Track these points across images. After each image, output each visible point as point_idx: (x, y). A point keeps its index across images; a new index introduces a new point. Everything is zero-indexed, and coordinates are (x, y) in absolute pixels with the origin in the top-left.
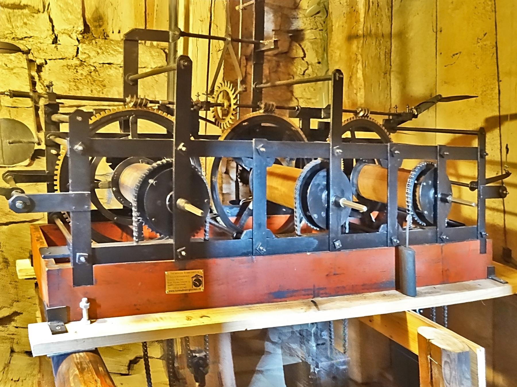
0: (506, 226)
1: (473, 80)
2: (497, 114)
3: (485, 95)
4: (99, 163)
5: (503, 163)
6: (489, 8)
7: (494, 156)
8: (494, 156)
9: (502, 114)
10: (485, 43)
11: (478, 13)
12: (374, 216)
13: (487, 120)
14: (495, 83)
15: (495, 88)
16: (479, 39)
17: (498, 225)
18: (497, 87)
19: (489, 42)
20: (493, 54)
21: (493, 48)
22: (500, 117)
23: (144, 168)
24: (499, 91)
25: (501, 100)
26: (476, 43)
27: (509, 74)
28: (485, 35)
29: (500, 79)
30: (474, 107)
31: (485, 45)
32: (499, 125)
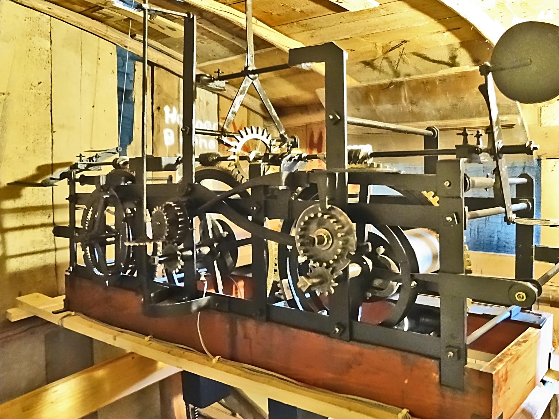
0: (57, 261)
1: (24, 127)
2: (50, 162)
3: (38, 143)
4: (24, 295)
5: (54, 206)
6: (45, 57)
7: (46, 201)
8: (46, 201)
9: (54, 162)
10: (39, 92)
11: (33, 57)
12: (83, 264)
13: (39, 168)
14: (48, 133)
15: (49, 138)
16: (32, 86)
17: (31, 268)
18: (51, 137)
19: (45, 92)
20: (48, 105)
21: (48, 99)
22: (52, 164)
23: (337, 332)
24: (52, 140)
25: (53, 148)
26: (29, 89)
27: (62, 126)
28: (39, 83)
29: (54, 130)
30: (24, 155)
31: (39, 94)
32: (51, 172)
